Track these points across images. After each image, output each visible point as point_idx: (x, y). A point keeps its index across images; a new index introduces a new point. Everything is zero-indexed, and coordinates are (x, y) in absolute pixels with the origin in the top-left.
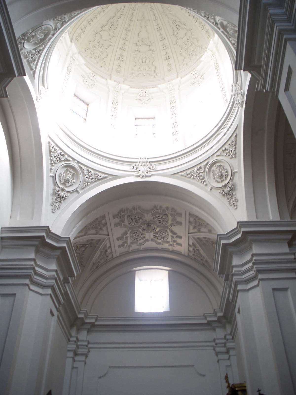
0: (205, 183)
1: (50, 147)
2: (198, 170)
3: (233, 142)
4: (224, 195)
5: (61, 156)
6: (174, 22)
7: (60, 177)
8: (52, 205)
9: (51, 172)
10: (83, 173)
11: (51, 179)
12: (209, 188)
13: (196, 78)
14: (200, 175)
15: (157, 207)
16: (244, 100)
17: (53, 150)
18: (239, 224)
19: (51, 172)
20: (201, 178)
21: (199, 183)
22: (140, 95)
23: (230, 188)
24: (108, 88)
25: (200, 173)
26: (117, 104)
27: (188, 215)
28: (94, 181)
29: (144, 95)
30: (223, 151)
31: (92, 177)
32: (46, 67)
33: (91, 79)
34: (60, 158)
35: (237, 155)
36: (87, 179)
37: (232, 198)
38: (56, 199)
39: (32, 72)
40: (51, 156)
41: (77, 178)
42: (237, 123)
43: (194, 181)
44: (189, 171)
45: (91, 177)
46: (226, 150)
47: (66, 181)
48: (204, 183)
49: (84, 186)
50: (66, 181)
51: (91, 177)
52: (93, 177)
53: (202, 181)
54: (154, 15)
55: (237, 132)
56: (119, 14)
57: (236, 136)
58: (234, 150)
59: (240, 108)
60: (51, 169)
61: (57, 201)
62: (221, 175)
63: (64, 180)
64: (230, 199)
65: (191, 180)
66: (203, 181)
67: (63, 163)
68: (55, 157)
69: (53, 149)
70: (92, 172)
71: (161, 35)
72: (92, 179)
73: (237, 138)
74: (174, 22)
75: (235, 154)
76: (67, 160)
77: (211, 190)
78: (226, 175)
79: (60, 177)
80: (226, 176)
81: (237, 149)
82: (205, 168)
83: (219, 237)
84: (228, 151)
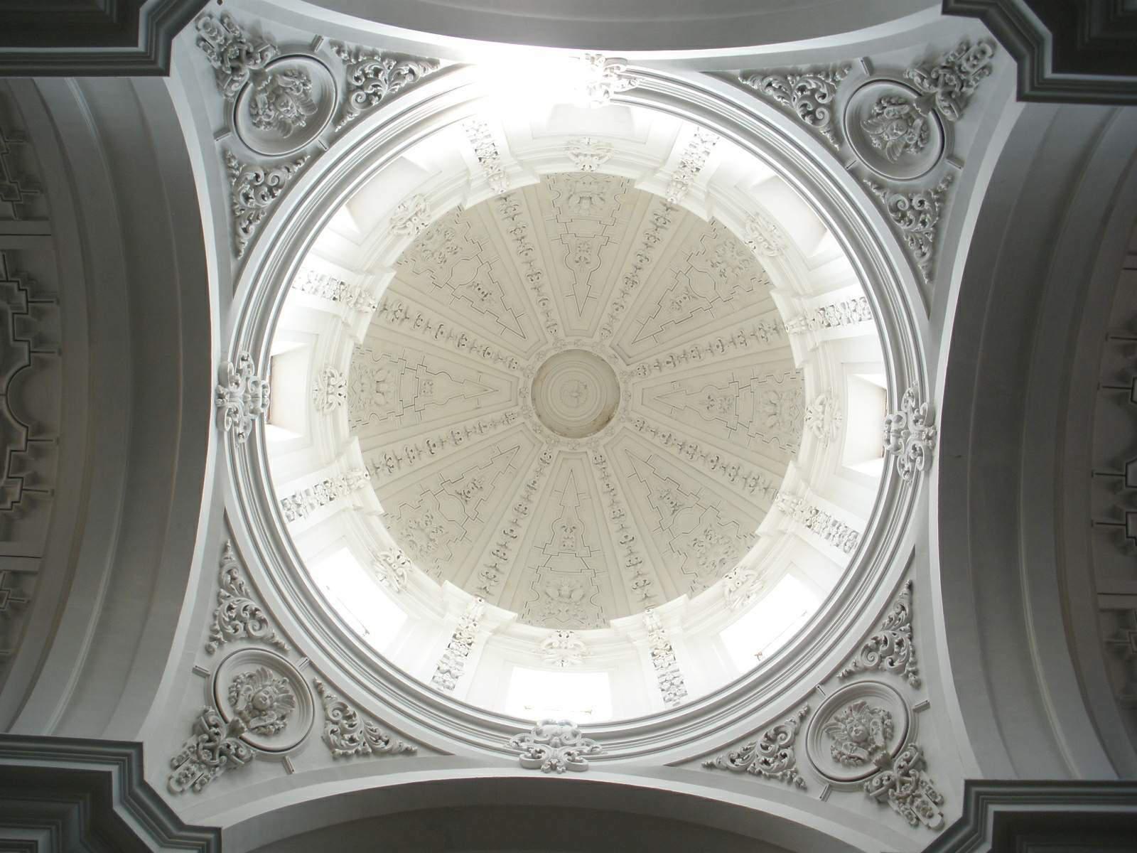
0: (214, 645)
1: (417, 60)
2: (253, 614)
3: (387, 743)
4: (197, 729)
5: (368, 95)
6: (477, 486)
7: (299, 74)
8: (226, 20)
10: (277, 166)
11: (308, 37)
13: (390, 565)
14: (237, 622)
15: (41, 438)
16: (559, 773)
17: (405, 70)
18: (211, 836)
19: (332, 44)
20: (231, 631)
21: (209, 620)
22: (333, 376)
24: (370, 272)
26: (334, 299)
27: (13, 568)
28: (236, 204)
29: (331, 389)
30: (343, 708)
31: (253, 197)
32: (686, 110)
33: (410, 219)
34: (361, 88)
35: (343, 763)
36: (251, 176)
37: (203, 766)
38: (237, 41)
40: (383, 60)
41: (267, 141)
43: (212, 604)
44: (241, 578)
46: (349, 718)
47: (278, 96)
48: (213, 639)
49: (234, 163)
50: (276, 95)
53: (217, 632)
54: (494, 424)
55: (422, 754)
57: (408, 752)
58: (360, 748)
59: (516, 759)
61: (231, 45)
62: (260, 711)
63: (284, 89)
64: (195, 758)
65: (214, 587)
66: (220, 636)
68: (377, 72)
69: (405, 70)
70: (269, 201)
72: (247, 198)
74: (477, 486)
75: (345, 756)
76: (339, 117)
77: (197, 671)
78: (264, 727)
79: (297, 74)
80: (263, 729)
81: (362, 761)
83: (133, 751)
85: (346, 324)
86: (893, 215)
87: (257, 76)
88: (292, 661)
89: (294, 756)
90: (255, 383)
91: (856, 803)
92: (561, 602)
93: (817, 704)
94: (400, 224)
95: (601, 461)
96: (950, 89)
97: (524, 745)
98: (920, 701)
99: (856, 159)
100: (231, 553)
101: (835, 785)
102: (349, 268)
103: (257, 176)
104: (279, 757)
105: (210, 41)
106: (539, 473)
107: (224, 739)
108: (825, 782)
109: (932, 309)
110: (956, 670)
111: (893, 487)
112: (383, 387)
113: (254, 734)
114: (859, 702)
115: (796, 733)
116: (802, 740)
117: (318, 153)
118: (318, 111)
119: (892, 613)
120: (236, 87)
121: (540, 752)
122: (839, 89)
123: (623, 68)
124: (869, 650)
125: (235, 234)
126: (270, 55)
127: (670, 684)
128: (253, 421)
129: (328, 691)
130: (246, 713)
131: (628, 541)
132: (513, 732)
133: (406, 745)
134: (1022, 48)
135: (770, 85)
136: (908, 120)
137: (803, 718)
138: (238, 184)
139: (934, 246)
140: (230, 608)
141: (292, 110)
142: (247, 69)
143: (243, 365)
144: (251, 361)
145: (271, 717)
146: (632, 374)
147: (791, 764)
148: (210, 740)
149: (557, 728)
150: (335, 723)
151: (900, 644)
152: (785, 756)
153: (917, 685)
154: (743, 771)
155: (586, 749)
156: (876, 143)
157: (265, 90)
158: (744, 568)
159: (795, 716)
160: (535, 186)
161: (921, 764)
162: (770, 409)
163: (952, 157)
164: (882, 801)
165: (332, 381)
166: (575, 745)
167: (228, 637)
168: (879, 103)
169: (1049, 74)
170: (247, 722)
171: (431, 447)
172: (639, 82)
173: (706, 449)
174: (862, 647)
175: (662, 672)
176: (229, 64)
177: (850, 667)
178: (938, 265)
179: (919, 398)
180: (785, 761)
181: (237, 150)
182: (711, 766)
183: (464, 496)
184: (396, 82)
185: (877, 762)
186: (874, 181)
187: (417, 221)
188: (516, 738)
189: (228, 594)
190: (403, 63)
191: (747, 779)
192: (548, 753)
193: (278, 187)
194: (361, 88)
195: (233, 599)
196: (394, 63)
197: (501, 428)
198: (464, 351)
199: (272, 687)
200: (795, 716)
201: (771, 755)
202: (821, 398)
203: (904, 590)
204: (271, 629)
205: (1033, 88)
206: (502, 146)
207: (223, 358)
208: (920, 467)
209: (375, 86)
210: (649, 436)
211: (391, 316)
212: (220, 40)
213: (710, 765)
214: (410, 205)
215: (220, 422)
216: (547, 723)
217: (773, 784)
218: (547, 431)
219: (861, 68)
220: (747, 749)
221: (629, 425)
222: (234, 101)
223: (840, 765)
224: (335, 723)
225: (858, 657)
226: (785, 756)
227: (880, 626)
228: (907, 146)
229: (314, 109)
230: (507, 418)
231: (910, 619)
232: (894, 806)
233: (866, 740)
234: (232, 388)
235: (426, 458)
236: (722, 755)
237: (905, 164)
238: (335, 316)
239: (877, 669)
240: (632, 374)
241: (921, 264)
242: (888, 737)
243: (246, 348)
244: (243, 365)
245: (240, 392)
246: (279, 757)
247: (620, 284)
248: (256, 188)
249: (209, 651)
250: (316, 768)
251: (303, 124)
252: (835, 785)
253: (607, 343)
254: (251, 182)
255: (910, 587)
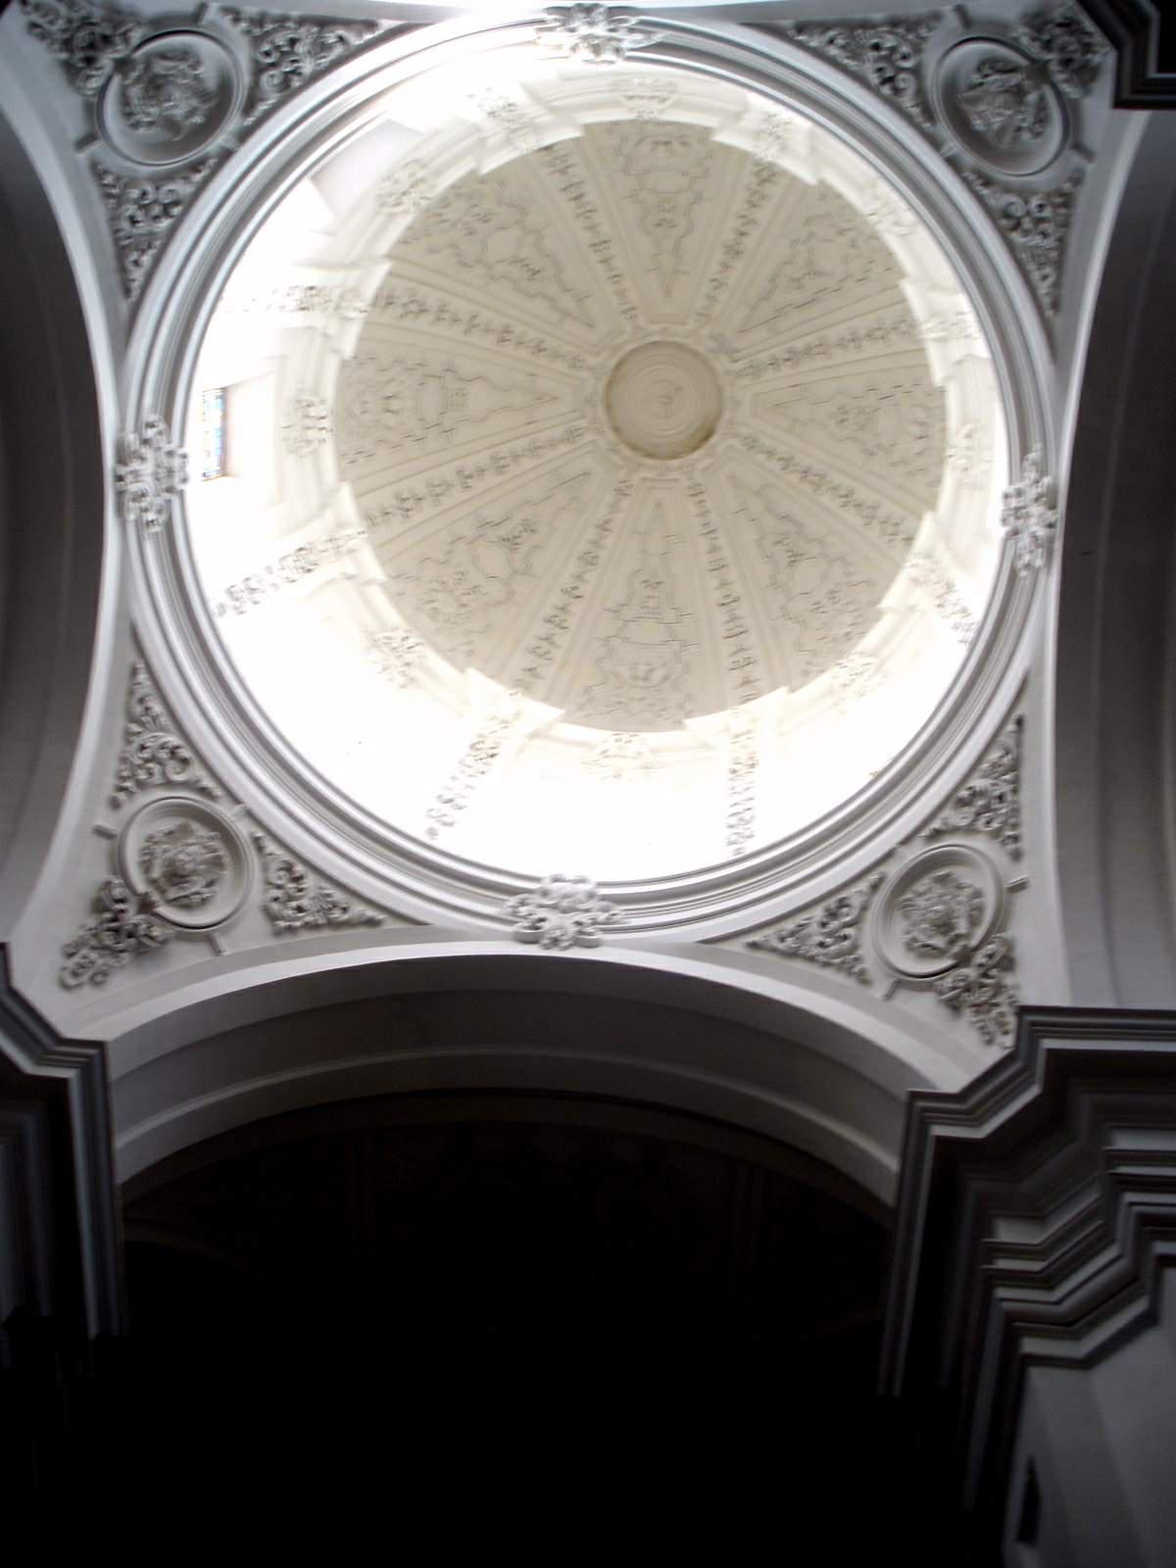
0: (122, 796)
1: (347, 23)
4: (99, 906)
6: (529, 527)
7: (184, 55)
9: (226, 10)
10: (170, 176)
12: (107, 820)
17: (331, 38)
19: (226, 10)
20: (142, 775)
21: (113, 765)
23: (146, 935)
25: (160, 762)
30: (289, 868)
34: (273, 65)
35: (288, 940)
36: (135, 193)
38: (86, 22)
39: (787, 23)
42: (439, 923)
43: (118, 745)
44: (157, 708)
45: (140, 216)
46: (297, 879)
47: (158, 88)
50: (155, 86)
51: (140, 216)
52: (142, 228)
53: (124, 779)
54: (553, 444)
55: (391, 925)
56: (567, 302)
57: (371, 923)
60: (237, 20)
65: (120, 723)
66: (128, 784)
67: (246, 79)
68: (293, 42)
69: (331, 38)
71: (481, 471)
72: (133, 221)
73: (362, 930)
75: (290, 930)
76: (249, 107)
77: (101, 832)
78: (186, 897)
82: (185, 785)
84: (291, 892)
85: (326, 336)
86: (1006, 223)
87: (123, 65)
88: (225, 811)
89: (224, 932)
90: (170, 454)
91: (924, 1006)
92: (634, 686)
93: (894, 870)
94: (392, 200)
95: (697, 492)
96: (1068, 56)
97: (523, 910)
98: (1016, 879)
99: (954, 145)
100: (142, 677)
101: (903, 982)
102: (321, 265)
103: (144, 194)
104: (204, 936)
105: (46, 26)
106: (614, 507)
107: (132, 917)
108: (892, 976)
109: (1057, 350)
110: (1061, 842)
111: (1012, 586)
112: (394, 405)
113: (174, 906)
114: (942, 872)
115: (864, 908)
116: (871, 916)
117: (226, 155)
118: (217, 102)
119: (994, 755)
120: (95, 84)
121: (542, 920)
122: (927, 46)
123: (633, 20)
124: (963, 803)
125: (123, 270)
126: (136, 36)
127: (740, 820)
128: (169, 502)
129: (271, 847)
130: (163, 882)
131: (729, 602)
132: (512, 891)
133: (371, 913)
134: (1122, 31)
135: (831, 41)
136: (1019, 93)
137: (875, 887)
138: (119, 205)
139: (1059, 265)
140: (143, 748)
141: (180, 105)
142: (106, 60)
143: (150, 433)
144: (162, 426)
145: (195, 883)
146: (739, 374)
147: (854, 948)
148: (115, 920)
149: (567, 887)
150: (279, 887)
151: (1001, 798)
152: (845, 938)
153: (1017, 856)
154: (792, 954)
155: (602, 917)
156: (978, 124)
157: (138, 80)
158: (862, 653)
159: (863, 885)
160: (577, 140)
161: (1007, 963)
162: (916, 430)
163: (1079, 147)
164: (954, 1006)
165: (312, 412)
166: (587, 911)
167: (142, 785)
168: (979, 69)
169: (1153, 73)
170: (163, 892)
171: (465, 477)
172: (659, 36)
173: (836, 478)
174: (955, 800)
175: (737, 798)
176: (79, 55)
177: (936, 824)
178: (1065, 292)
179: (1043, 469)
180: (846, 943)
181: (111, 161)
182: (754, 946)
183: (511, 542)
184: (322, 54)
185: (955, 956)
186: (980, 174)
187: (415, 195)
188: (513, 900)
189: (140, 730)
190: (327, 29)
191: (798, 965)
192: (554, 921)
193: (176, 203)
194: (273, 65)
195: (147, 736)
196: (315, 29)
197: (563, 448)
198: (509, 348)
199: (194, 850)
200: (863, 885)
201: (829, 935)
202: (968, 427)
203: (1011, 727)
204: (197, 772)
205: (1135, 92)
206: (520, 98)
207: (122, 428)
208: (1039, 563)
209: (294, 61)
210: (761, 457)
211: (400, 311)
212: (61, 24)
213: (755, 943)
214: (403, 176)
215: (120, 510)
216: (556, 880)
217: (829, 974)
218: (626, 452)
219: (952, 21)
220: (801, 926)
221: (737, 443)
222: (96, 100)
223: (912, 955)
224: (279, 887)
225: (947, 812)
226: (845, 938)
227: (977, 774)
228: (1019, 129)
229: (209, 100)
230: (571, 436)
231: (1015, 767)
232: (968, 1014)
233: (945, 925)
234: (135, 465)
235: (458, 495)
236: (769, 931)
237: (1012, 156)
238: (309, 328)
239: (970, 830)
240: (739, 374)
241: (1043, 288)
242: (974, 922)
243: (154, 410)
244: (150, 433)
245: (147, 468)
246: (204, 936)
247: (719, 255)
248: (142, 207)
249: (115, 804)
250: (252, 946)
251: (198, 119)
252: (903, 982)
253: (706, 331)
254: (136, 202)
255: (1020, 722)
